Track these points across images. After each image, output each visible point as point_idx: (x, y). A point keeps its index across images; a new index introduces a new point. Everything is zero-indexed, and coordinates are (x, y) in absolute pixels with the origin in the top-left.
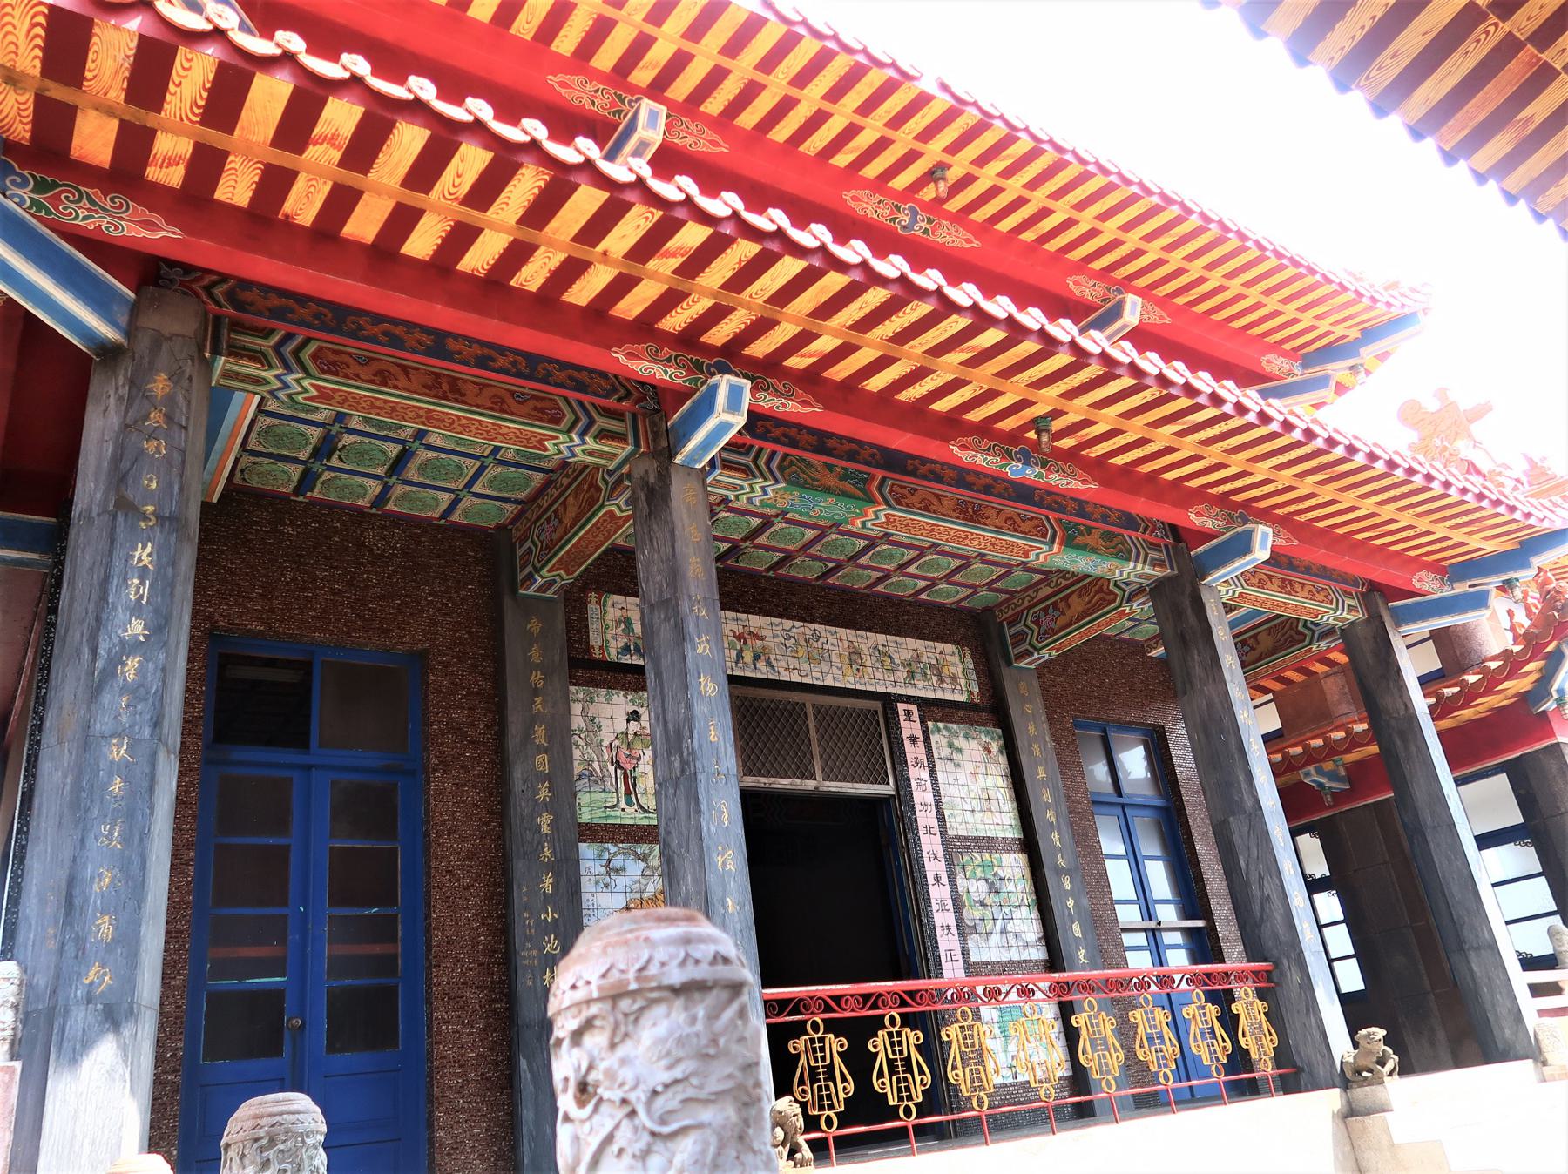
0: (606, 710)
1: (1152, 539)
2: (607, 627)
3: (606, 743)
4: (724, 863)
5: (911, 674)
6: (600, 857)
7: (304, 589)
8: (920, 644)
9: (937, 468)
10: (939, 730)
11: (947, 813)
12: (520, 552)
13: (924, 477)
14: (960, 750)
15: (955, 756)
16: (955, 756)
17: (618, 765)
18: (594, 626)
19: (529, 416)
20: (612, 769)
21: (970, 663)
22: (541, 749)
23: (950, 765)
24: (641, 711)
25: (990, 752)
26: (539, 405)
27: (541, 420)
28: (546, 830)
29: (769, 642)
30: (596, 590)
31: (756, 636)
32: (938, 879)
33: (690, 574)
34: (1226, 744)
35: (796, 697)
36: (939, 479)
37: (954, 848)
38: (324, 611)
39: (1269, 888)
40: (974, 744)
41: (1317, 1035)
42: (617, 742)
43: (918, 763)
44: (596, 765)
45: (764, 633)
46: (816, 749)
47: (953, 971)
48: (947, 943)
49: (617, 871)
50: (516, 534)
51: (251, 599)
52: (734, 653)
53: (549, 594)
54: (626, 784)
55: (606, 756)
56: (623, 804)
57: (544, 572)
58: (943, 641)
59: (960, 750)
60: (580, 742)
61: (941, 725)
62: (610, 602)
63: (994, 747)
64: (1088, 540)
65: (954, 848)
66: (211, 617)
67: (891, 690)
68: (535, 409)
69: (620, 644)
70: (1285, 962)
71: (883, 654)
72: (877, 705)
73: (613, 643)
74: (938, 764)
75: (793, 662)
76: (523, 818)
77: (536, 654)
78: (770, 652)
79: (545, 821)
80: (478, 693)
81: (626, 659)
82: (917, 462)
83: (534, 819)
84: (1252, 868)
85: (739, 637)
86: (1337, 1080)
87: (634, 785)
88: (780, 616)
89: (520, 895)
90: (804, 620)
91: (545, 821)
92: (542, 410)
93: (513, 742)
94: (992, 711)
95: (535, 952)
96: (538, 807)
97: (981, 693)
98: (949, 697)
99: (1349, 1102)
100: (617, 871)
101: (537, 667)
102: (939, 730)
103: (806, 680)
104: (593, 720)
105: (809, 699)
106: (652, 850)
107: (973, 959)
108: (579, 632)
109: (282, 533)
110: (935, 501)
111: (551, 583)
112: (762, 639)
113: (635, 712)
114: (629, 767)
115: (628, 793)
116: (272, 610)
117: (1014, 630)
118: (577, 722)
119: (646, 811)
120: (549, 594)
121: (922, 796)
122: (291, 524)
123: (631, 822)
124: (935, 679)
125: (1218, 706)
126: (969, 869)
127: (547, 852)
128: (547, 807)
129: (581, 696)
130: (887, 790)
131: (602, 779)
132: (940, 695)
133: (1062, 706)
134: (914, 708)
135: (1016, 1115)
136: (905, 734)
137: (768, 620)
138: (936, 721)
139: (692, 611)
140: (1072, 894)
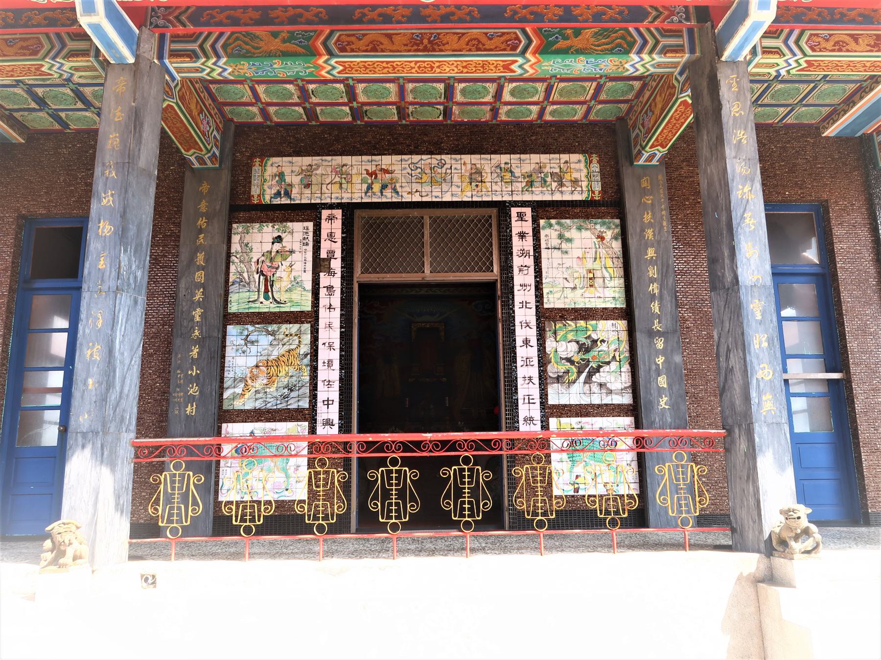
0: (257, 237)
1: (667, 25)
2: (265, 181)
3: (254, 260)
4: (92, 355)
5: (531, 184)
7: (70, 185)
9: (389, 10)
10: (551, 225)
11: (545, 291)
13: (372, 21)
14: (570, 240)
15: (564, 246)
16: (564, 246)
17: (262, 273)
18: (255, 181)
19: (16, 54)
20: (257, 276)
21: (596, 167)
23: (557, 253)
24: (283, 235)
25: (603, 238)
26: (25, 44)
27: (24, 55)
28: (198, 319)
29: (397, 174)
30: (260, 157)
31: (386, 171)
32: (526, 342)
33: (109, 147)
34: (718, 221)
35: (416, 213)
36: (387, 19)
38: (80, 197)
39: (734, 361)
40: (586, 234)
41: (752, 502)
42: (263, 258)
43: (523, 254)
44: (245, 275)
46: (427, 249)
48: (527, 390)
49: (252, 343)
51: (40, 196)
52: (365, 186)
54: (266, 286)
55: (254, 268)
56: (262, 299)
59: (570, 240)
60: (236, 260)
61: (553, 221)
62: (269, 163)
64: (577, 42)
65: (546, 317)
66: (18, 209)
67: (507, 198)
68: (22, 48)
69: (274, 191)
70: (737, 431)
72: (494, 211)
73: (268, 191)
74: (544, 254)
75: (416, 187)
76: (183, 312)
77: (203, 206)
78: (397, 182)
81: (277, 201)
82: (366, 11)
83: (190, 312)
84: (723, 340)
85: (370, 174)
86: (762, 545)
87: (272, 286)
88: (411, 153)
89: (176, 359)
92: (26, 48)
96: (193, 305)
97: (604, 191)
98: (567, 197)
99: (770, 568)
100: (252, 343)
102: (551, 225)
103: (425, 199)
104: (247, 245)
107: (551, 402)
109: (60, 153)
110: (385, 41)
112: (391, 172)
113: (279, 237)
114: (269, 274)
115: (266, 291)
116: (51, 201)
117: (208, 162)
118: (235, 247)
119: (278, 303)
122: (66, 148)
124: (554, 185)
125: (717, 184)
126: (560, 334)
127: (197, 333)
129: (240, 230)
131: (249, 284)
132: (557, 197)
134: (528, 211)
135: (578, 517)
137: (399, 157)
138: (549, 218)
139: (103, 174)
140: (664, 352)
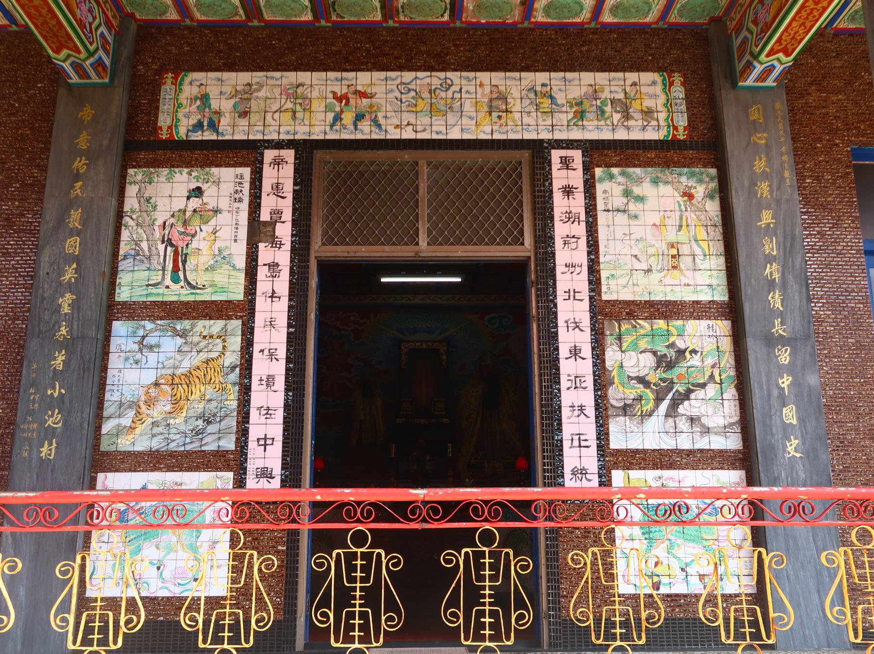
2: (180, 106)
3: (159, 222)
5: (581, 115)
8: (601, 78)
10: (611, 177)
11: (604, 275)
12: (737, 43)
14: (640, 199)
15: (632, 207)
16: (632, 207)
17: (170, 243)
18: (165, 107)
20: (161, 247)
21: (679, 92)
23: (621, 218)
25: (691, 197)
28: (66, 309)
31: (363, 95)
32: (575, 352)
35: (407, 156)
37: (605, 314)
40: (666, 190)
42: (172, 220)
43: (570, 217)
44: (144, 245)
45: (374, 90)
46: (424, 211)
47: (579, 459)
48: (577, 427)
49: (151, 348)
50: (731, 25)
52: (330, 116)
53: (770, 82)
54: (175, 261)
55: (158, 234)
56: (168, 281)
57: (762, 57)
58: (639, 70)
59: (640, 199)
60: (131, 223)
61: (615, 171)
62: (187, 80)
63: (700, 191)
65: (605, 314)
67: (545, 136)
69: (193, 121)
71: (293, 93)
72: (525, 155)
74: (602, 218)
75: (407, 117)
77: (83, 141)
78: (379, 109)
79: (66, 302)
80: (32, 185)
81: (197, 136)
83: (54, 299)
87: (184, 262)
90: (431, 69)
91: (66, 302)
94: (702, 146)
95: (35, 426)
96: (60, 288)
97: (691, 126)
100: (151, 348)
104: (148, 200)
105: (423, 158)
111: (770, 70)
114: (181, 244)
115: (176, 269)
119: (193, 287)
120: (770, 82)
121: (569, 256)
123: (174, 298)
124: (617, 117)
126: (628, 340)
127: (64, 331)
129: (139, 177)
130: (527, 247)
131: (149, 258)
132: (621, 135)
133: (834, 132)
136: (557, 184)
138: (609, 166)
140: (790, 369)
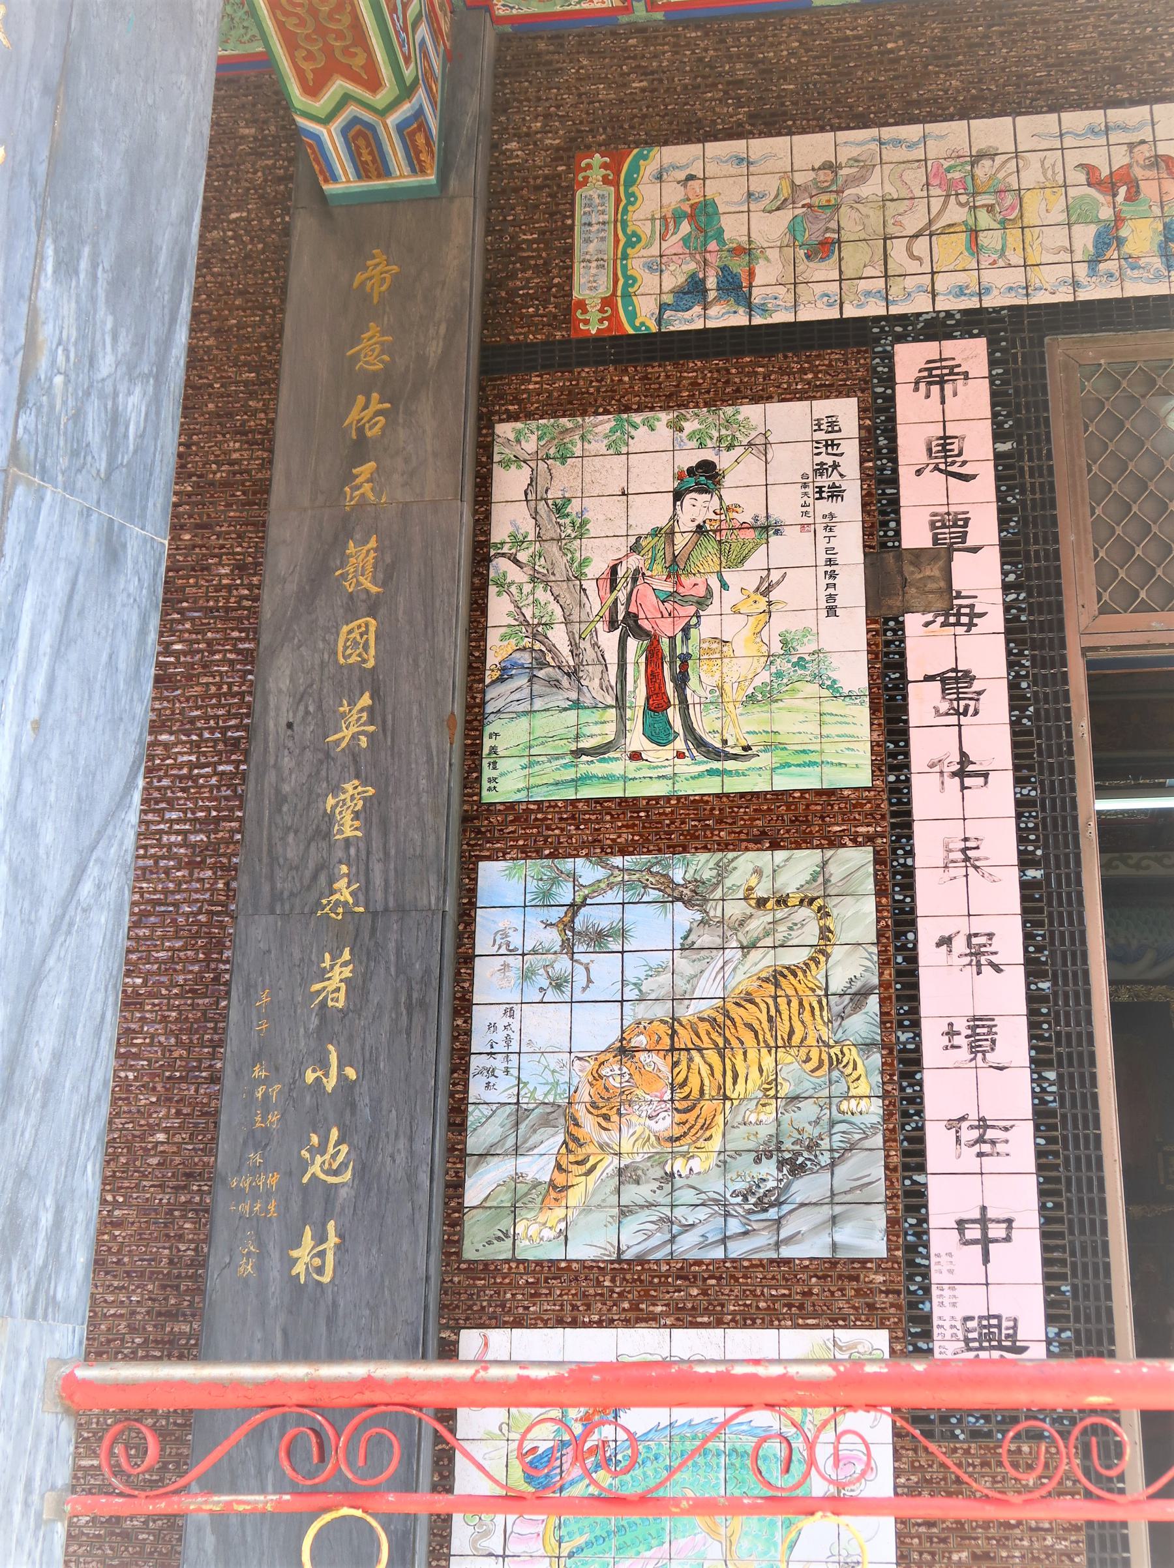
0: (608, 473)
2: (634, 240)
3: (598, 567)
6: (545, 900)
17: (631, 626)
22: (354, 606)
28: (348, 828)
30: (605, 147)
42: (634, 561)
44: (559, 636)
49: (598, 938)
52: (1085, 236)
54: (654, 680)
55: (595, 603)
56: (636, 740)
60: (515, 574)
62: (649, 168)
69: (674, 279)
73: (648, 282)
76: (280, 799)
79: (346, 806)
80: (225, 484)
81: (690, 320)
83: (312, 797)
87: (681, 680)
93: (279, 591)
95: (273, 1180)
96: (327, 767)
100: (598, 938)
101: (368, 384)
104: (559, 509)
106: (722, 871)
108: (544, 269)
114: (666, 628)
115: (656, 703)
123: (659, 789)
127: (344, 891)
128: (356, 763)
131: (574, 674)
